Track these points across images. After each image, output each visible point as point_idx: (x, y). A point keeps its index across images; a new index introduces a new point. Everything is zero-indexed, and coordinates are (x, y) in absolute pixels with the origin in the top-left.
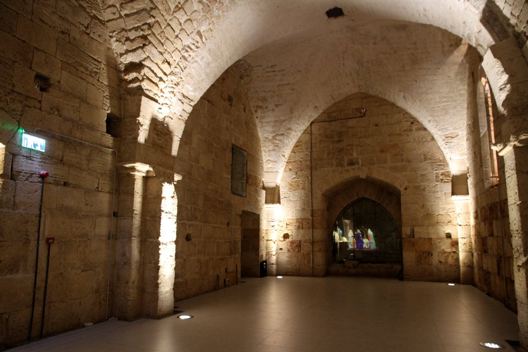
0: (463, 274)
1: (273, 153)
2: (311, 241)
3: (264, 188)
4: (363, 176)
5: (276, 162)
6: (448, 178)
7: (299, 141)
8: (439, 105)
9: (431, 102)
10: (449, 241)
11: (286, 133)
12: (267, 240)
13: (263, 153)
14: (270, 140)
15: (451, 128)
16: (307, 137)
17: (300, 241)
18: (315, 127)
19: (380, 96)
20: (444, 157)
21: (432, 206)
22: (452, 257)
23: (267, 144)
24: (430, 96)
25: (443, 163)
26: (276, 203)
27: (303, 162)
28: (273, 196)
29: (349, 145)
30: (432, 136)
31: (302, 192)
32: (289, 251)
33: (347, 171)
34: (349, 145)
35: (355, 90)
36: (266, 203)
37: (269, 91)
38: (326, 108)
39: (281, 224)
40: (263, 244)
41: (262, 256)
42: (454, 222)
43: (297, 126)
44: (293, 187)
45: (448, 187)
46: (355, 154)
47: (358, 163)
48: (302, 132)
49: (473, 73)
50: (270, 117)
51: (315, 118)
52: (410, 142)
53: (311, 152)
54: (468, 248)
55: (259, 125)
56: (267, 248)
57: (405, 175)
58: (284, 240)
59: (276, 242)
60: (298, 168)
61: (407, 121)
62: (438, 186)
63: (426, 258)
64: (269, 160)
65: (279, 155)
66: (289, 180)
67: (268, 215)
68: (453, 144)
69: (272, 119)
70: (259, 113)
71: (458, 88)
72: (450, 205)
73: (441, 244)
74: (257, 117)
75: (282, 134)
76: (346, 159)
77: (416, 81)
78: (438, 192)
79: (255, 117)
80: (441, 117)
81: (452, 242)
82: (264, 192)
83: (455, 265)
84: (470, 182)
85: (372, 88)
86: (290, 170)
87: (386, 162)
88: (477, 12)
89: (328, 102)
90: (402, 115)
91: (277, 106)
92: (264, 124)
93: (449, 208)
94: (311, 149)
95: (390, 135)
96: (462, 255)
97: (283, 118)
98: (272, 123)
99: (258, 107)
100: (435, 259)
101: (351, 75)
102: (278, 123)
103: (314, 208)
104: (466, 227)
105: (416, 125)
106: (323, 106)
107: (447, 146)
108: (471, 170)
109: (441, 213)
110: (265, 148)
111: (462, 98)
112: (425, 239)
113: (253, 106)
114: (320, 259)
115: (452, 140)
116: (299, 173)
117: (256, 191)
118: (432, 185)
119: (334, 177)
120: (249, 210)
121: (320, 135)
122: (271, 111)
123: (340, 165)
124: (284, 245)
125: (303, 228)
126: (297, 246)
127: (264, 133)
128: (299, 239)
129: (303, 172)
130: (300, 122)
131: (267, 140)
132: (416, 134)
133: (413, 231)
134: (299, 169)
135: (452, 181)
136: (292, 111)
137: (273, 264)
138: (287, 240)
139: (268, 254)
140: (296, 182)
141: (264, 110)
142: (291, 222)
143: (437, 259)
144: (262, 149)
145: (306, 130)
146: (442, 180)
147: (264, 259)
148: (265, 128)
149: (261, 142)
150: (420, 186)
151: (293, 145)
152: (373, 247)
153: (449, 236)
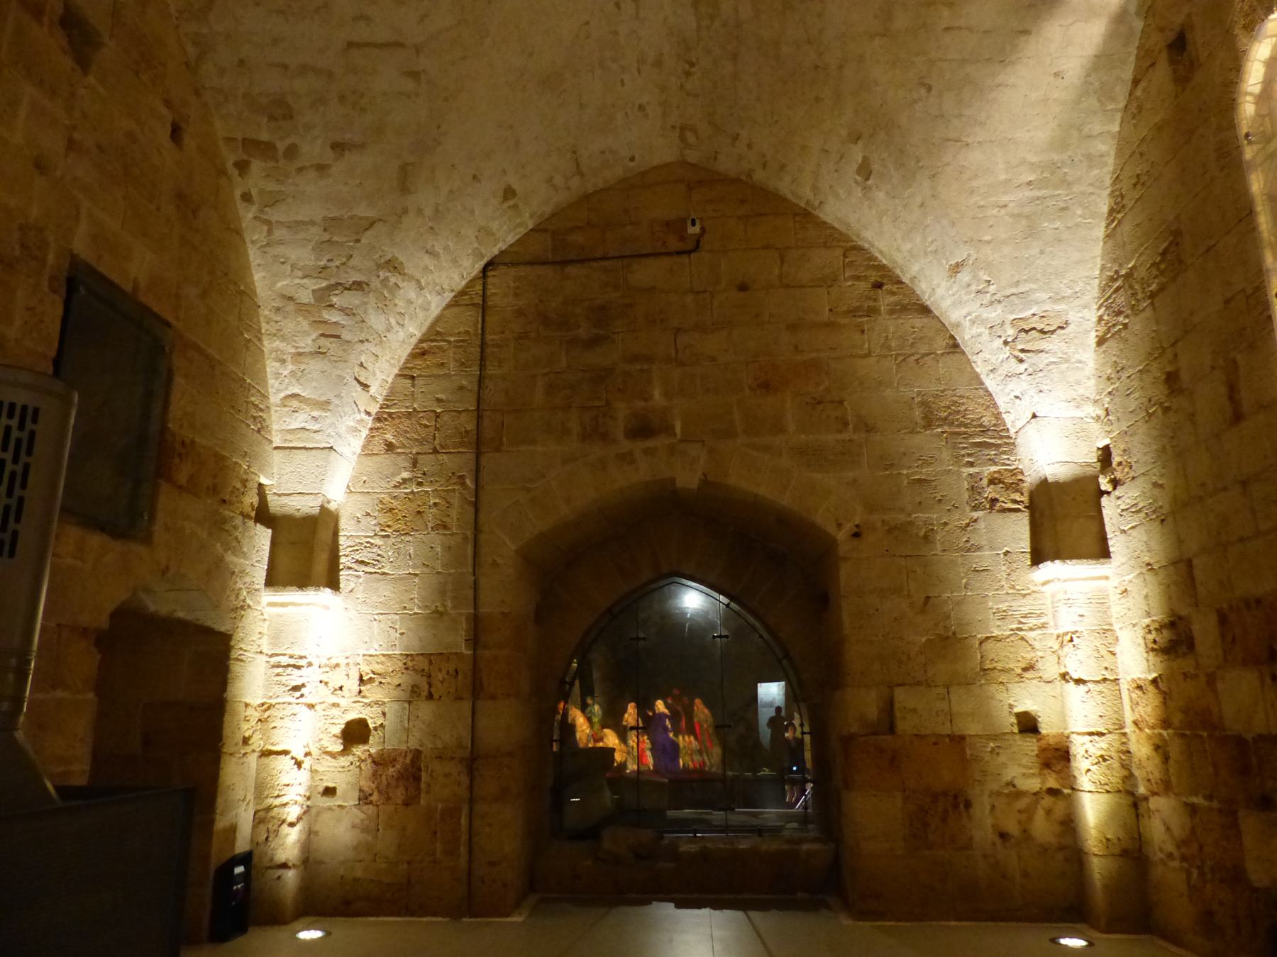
0: (1106, 886)
1: (314, 365)
2: (467, 753)
3: (263, 515)
4: (688, 479)
5: (325, 405)
6: (1017, 497)
7: (433, 333)
8: (1005, 199)
9: (975, 183)
10: (1030, 746)
11: (375, 283)
12: (266, 754)
13: (271, 366)
14: (302, 309)
15: (1045, 296)
16: (467, 320)
17: (417, 754)
18: (500, 283)
19: (759, 176)
20: (998, 416)
21: (958, 603)
22: (1049, 812)
23: (289, 326)
24: (974, 157)
25: (993, 437)
26: (317, 585)
27: (446, 418)
28: (308, 553)
29: (635, 358)
30: (952, 337)
31: (436, 540)
32: (364, 798)
33: (627, 458)
34: (635, 358)
35: (663, 151)
36: (271, 582)
37: (304, 70)
38: (548, 210)
39: (336, 679)
40: (239, 775)
41: (232, 830)
42: (1050, 669)
43: (427, 260)
44: (396, 518)
45: (1017, 532)
46: (657, 394)
47: (669, 430)
48: (449, 296)
49: (1179, 45)
50: (309, 200)
51: (502, 246)
52: (868, 355)
53: (481, 379)
54: (1115, 778)
55: (254, 236)
56: (261, 788)
57: (855, 481)
58: (345, 751)
59: (307, 763)
60: (421, 442)
61: (858, 278)
62: (981, 525)
63: (944, 820)
64: (294, 396)
65: (341, 378)
66: (382, 489)
67: (276, 638)
68: (1043, 360)
69: (313, 211)
70: (257, 178)
71: (1086, 130)
72: (1029, 600)
73: (1002, 759)
74: (247, 197)
75: (358, 286)
76: (622, 410)
77: (929, 89)
78: (979, 548)
79: (238, 193)
80: (1006, 250)
81: (1043, 750)
82: (262, 537)
83: (1061, 848)
84: (1117, 511)
85: (736, 138)
86: (390, 447)
87: (778, 428)
88: (513, 547)
89: (558, 180)
90: (839, 252)
91: (339, 147)
92: (279, 233)
93: (1025, 610)
94: (482, 367)
95: (793, 327)
96: (1093, 808)
97: (363, 211)
98: (314, 230)
99: (252, 145)
100: (983, 821)
101: (658, 63)
102: (343, 230)
103: (483, 610)
104: (1101, 687)
105: (893, 294)
106: (540, 200)
107: (1022, 367)
108: (1138, 455)
109: (996, 632)
110: (277, 344)
111: (1095, 172)
112: (937, 740)
113: (229, 140)
114: (503, 832)
115: (1044, 344)
116: (427, 462)
117: (220, 527)
118: (958, 519)
119: (575, 481)
120: (181, 614)
121: (520, 313)
122: (312, 174)
123: (596, 433)
124: (343, 772)
125: (430, 696)
126: (401, 777)
127: (275, 271)
128: (413, 744)
129: (444, 458)
130: (438, 249)
131: (291, 307)
132: (889, 326)
133: (889, 707)
134: (427, 448)
135: (1032, 507)
136: (405, 181)
137: (284, 866)
138: (359, 750)
139: (265, 818)
140: (410, 497)
141: (282, 162)
142: (378, 668)
143: (989, 821)
144: (268, 345)
145: (462, 293)
146: (994, 501)
147: (242, 846)
148: (280, 250)
149: (265, 312)
150: (912, 523)
151: (409, 350)
152: (713, 759)
153: (1028, 725)
